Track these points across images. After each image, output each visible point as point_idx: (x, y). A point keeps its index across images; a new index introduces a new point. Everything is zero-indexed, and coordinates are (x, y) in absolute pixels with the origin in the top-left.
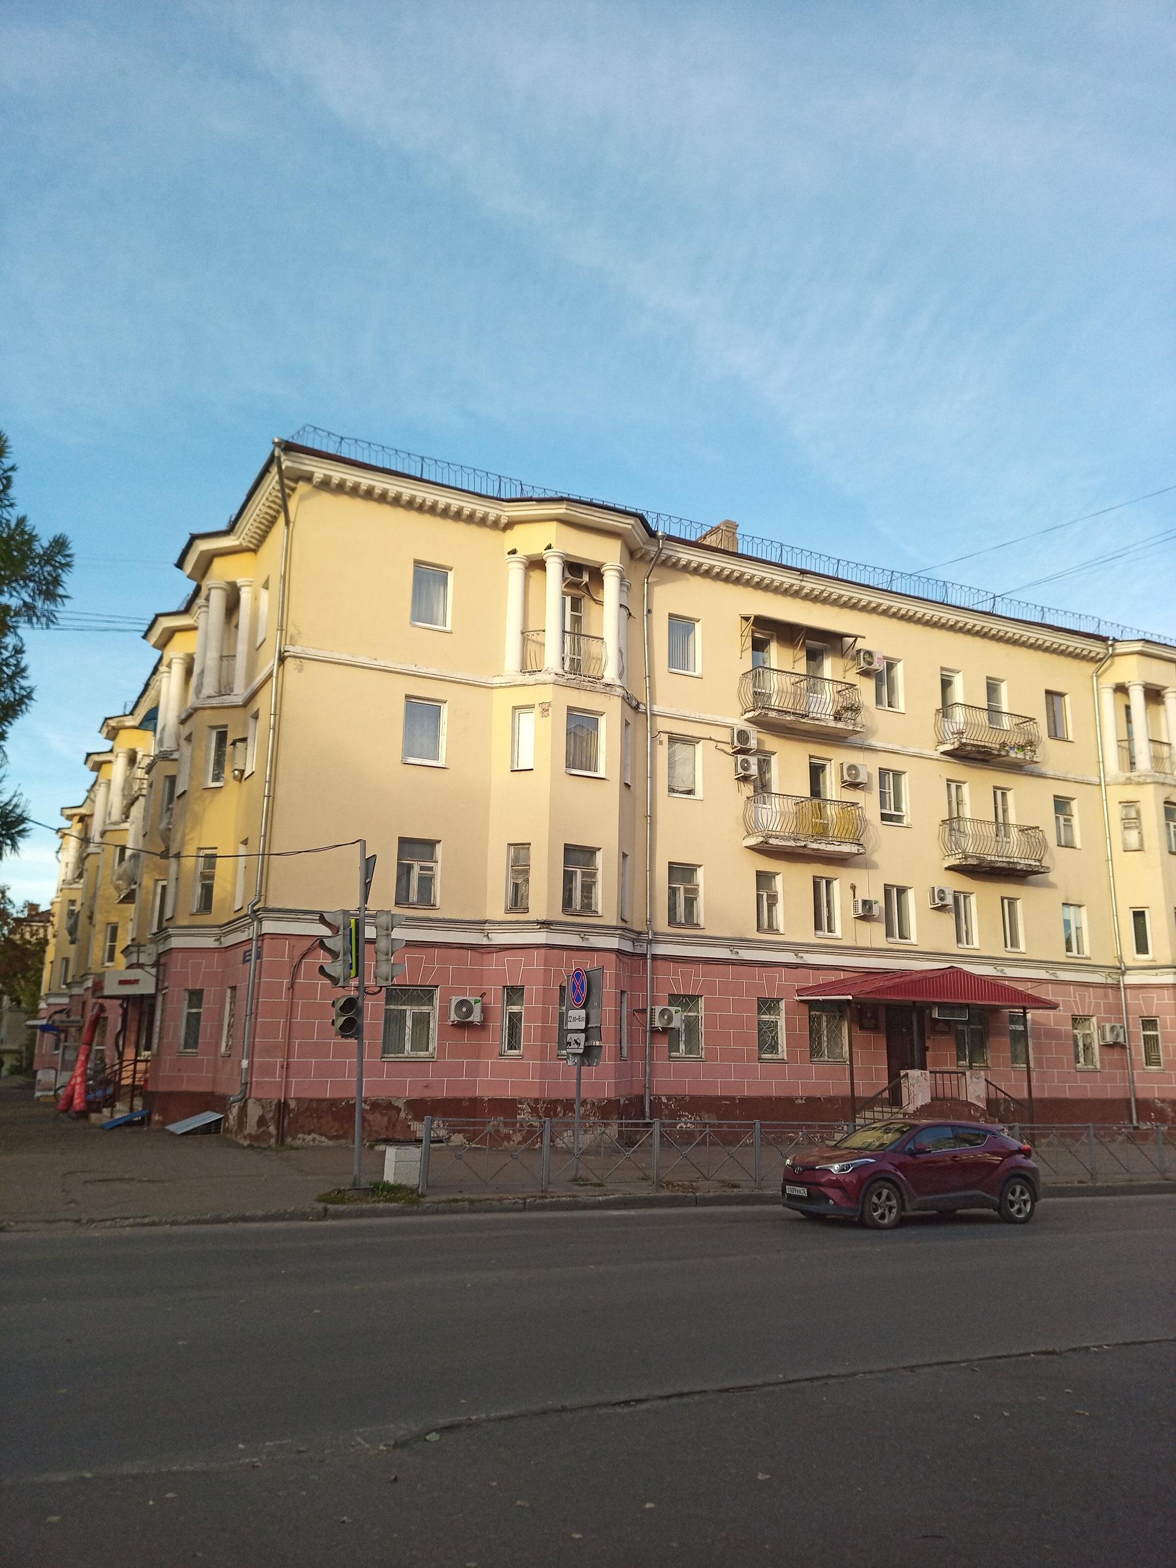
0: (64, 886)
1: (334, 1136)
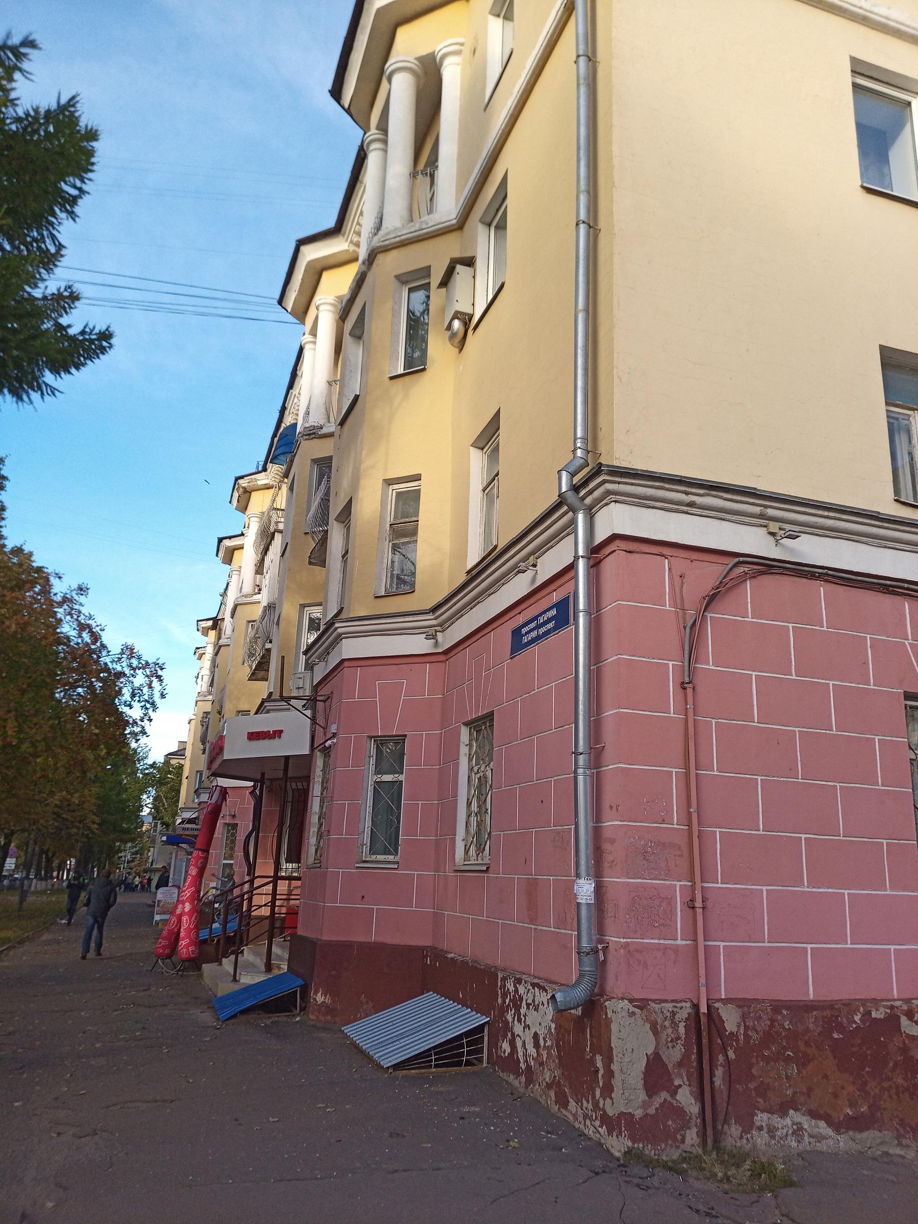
0: (199, 699)
1: (848, 1118)
